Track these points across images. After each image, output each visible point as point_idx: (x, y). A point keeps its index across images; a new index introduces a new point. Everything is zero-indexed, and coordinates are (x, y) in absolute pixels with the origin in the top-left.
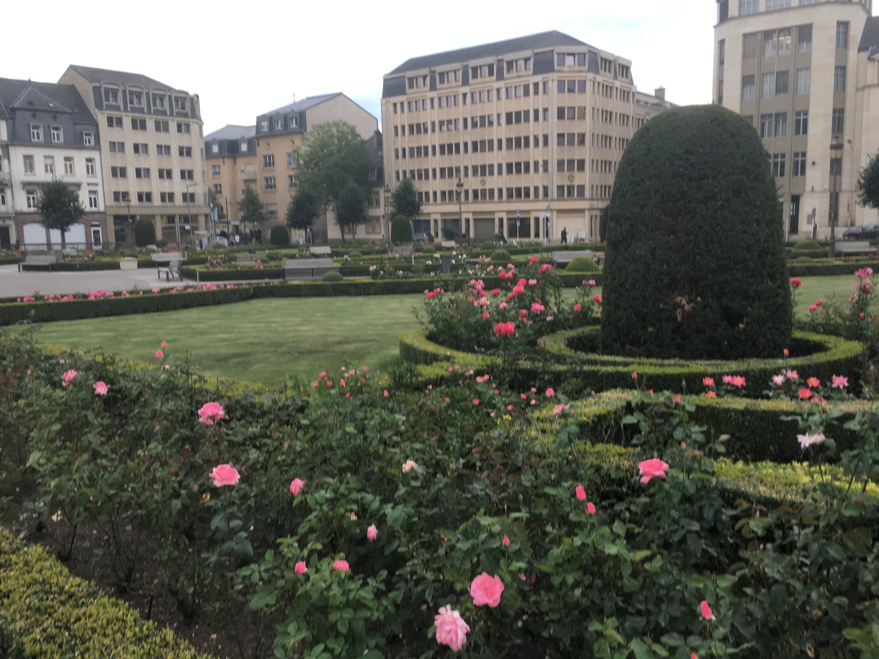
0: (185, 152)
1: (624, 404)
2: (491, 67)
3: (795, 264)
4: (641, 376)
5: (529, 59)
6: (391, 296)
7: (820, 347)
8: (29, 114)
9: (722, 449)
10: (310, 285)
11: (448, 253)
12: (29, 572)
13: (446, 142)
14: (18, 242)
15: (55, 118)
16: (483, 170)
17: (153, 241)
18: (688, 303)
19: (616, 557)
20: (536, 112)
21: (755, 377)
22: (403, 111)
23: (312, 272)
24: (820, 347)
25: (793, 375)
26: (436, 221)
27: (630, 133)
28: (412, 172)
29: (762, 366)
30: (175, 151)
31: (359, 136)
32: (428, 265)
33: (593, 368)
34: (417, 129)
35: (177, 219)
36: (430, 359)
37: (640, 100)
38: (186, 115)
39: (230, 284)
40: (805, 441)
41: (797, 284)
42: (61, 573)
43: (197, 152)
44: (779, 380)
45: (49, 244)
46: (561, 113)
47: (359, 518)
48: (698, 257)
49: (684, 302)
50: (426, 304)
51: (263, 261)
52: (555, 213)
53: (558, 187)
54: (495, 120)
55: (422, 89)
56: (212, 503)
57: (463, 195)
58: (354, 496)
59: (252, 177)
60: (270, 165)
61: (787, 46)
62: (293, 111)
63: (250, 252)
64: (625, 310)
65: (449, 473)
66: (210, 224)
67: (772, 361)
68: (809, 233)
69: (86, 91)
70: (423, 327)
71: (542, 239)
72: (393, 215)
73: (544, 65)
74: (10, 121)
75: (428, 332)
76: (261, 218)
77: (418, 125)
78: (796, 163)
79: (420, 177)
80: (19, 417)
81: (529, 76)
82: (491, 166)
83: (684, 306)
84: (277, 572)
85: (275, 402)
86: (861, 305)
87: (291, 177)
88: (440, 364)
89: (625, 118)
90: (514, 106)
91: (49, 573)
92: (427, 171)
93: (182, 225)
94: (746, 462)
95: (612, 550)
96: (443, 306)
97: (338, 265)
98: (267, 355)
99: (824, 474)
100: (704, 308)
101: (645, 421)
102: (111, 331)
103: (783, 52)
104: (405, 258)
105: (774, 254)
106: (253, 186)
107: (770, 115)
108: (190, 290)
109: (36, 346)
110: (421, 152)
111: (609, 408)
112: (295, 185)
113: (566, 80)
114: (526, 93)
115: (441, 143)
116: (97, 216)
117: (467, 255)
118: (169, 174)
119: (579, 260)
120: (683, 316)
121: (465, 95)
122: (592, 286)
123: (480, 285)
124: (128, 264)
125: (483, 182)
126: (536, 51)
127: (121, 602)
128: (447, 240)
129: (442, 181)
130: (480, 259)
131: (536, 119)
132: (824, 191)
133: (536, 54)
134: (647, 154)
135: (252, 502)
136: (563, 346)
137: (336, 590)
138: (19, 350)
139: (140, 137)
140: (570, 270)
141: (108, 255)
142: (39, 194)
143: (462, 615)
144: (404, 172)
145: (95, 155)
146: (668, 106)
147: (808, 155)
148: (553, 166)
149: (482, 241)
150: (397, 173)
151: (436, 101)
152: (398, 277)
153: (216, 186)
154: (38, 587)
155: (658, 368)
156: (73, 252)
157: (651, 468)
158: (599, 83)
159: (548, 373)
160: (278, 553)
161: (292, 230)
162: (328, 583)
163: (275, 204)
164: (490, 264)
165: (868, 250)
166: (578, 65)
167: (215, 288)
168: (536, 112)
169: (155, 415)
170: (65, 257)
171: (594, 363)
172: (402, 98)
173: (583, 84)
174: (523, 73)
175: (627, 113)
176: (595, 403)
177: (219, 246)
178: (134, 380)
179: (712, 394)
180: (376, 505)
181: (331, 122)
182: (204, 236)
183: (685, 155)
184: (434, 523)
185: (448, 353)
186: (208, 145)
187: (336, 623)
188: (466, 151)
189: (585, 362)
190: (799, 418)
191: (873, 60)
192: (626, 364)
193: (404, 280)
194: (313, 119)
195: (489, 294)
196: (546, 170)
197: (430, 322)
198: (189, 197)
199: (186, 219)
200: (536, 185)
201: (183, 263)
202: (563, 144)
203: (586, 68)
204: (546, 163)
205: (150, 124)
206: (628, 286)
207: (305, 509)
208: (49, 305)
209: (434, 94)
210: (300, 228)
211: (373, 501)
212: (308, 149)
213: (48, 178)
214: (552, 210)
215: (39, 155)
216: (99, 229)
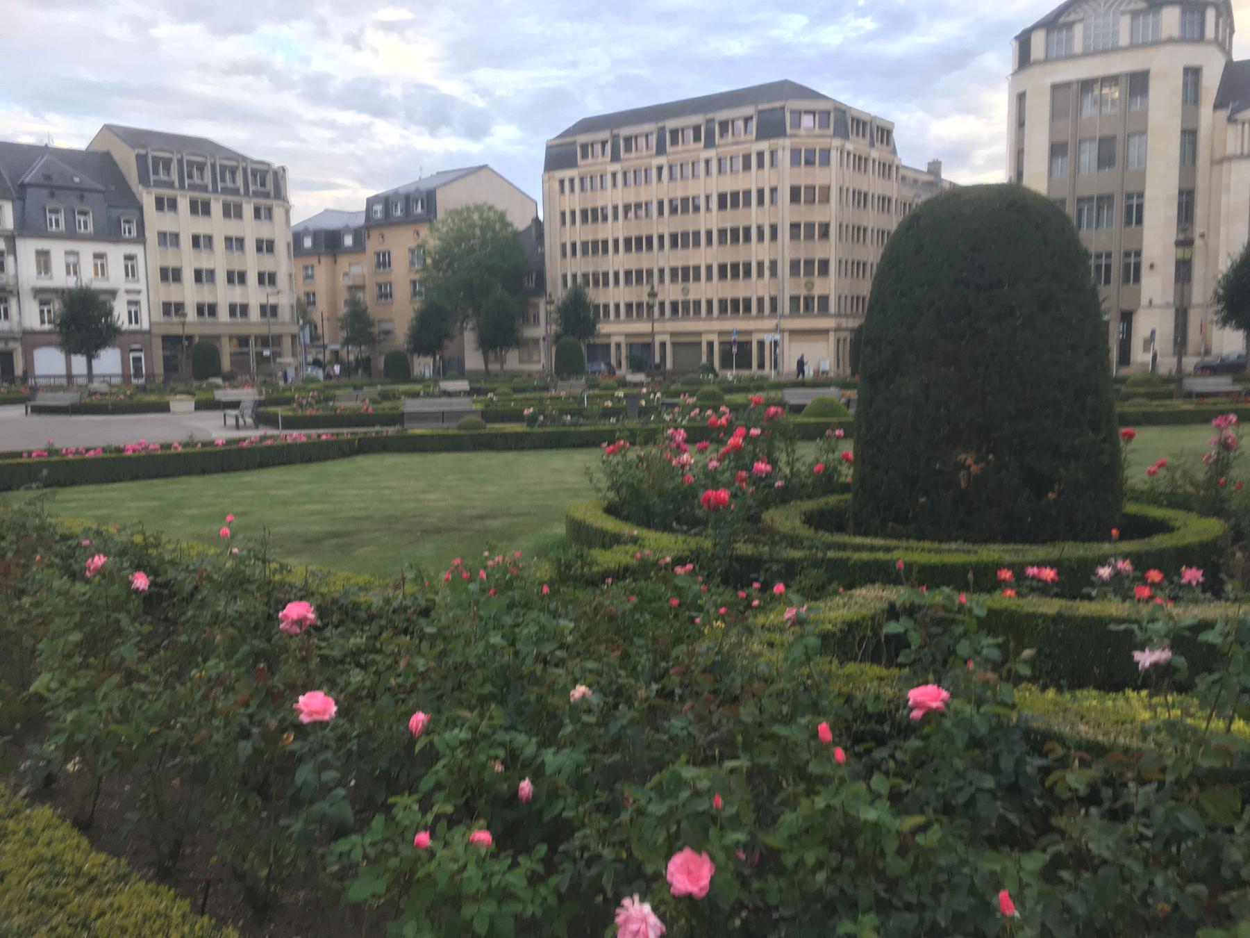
0: (264, 246)
1: (886, 606)
6: (554, 451)
7: (1162, 527)
8: (45, 192)
10: (439, 436)
11: (635, 391)
12: (32, 845)
13: (633, 235)
14: (25, 373)
15: (82, 198)
16: (686, 274)
17: (217, 372)
18: (976, 462)
20: (761, 193)
22: (572, 190)
23: (443, 416)
24: (1162, 527)
25: (1125, 566)
26: (618, 346)
27: (892, 222)
28: (585, 276)
29: (1081, 552)
30: (250, 245)
31: (511, 225)
33: (840, 554)
34: (592, 215)
35: (252, 341)
36: (610, 541)
37: (906, 178)
38: (267, 195)
39: (325, 434)
40: (1145, 659)
41: (1130, 437)
42: (78, 846)
43: (281, 247)
44: (1105, 572)
45: (70, 376)
46: (795, 194)
47: (507, 768)
49: (969, 461)
51: (373, 401)
52: (786, 335)
56: (296, 746)
58: (501, 736)
59: (359, 282)
60: (384, 266)
61: (1113, 101)
62: (417, 190)
63: (355, 387)
65: (636, 704)
66: (299, 349)
68: (1144, 365)
69: (127, 160)
71: (768, 371)
72: (558, 337)
73: (771, 127)
74: (18, 203)
76: (371, 341)
77: (594, 211)
78: (1127, 266)
79: (596, 283)
80: (22, 622)
81: (751, 142)
83: (969, 467)
84: (388, 847)
85: (387, 601)
86: (1220, 466)
87: (414, 283)
88: (622, 547)
89: (885, 201)
90: (729, 184)
91: (62, 846)
92: (606, 275)
93: (259, 349)
94: (1060, 690)
95: (870, 814)
96: (629, 465)
97: (480, 407)
98: (377, 534)
102: (154, 499)
103: (1108, 110)
104: (575, 398)
106: (360, 295)
107: (1090, 199)
108: (269, 442)
109: (49, 520)
110: (597, 248)
111: (864, 612)
112: (420, 293)
114: (747, 166)
115: (626, 234)
116: (139, 337)
117: (663, 394)
118: (242, 278)
120: (969, 481)
121: (660, 169)
122: (839, 438)
124: (182, 405)
125: (685, 291)
127: (163, 889)
128: (633, 372)
129: (627, 289)
131: (761, 202)
132: (1167, 305)
133: (760, 113)
135: (353, 745)
136: (798, 522)
137: (472, 871)
138: (23, 526)
139: (202, 226)
141: (152, 391)
142: (57, 306)
143: (655, 909)
144: (574, 276)
145: (137, 250)
146: (947, 186)
148: (784, 269)
149: (684, 373)
150: (565, 277)
151: (620, 177)
152: (564, 424)
153: (308, 295)
154: (45, 867)
156: (104, 388)
158: (848, 154)
159: (778, 561)
160: (390, 819)
161: (415, 357)
162: (461, 863)
163: (391, 320)
164: (694, 407)
166: (820, 126)
167: (304, 439)
168: (761, 193)
169: (216, 620)
170: (92, 394)
171: (843, 547)
172: (573, 173)
173: (826, 154)
174: (742, 137)
175: (888, 194)
176: (845, 605)
177: (312, 380)
178: (187, 570)
180: (530, 749)
181: (472, 206)
182: (289, 365)
184: (614, 776)
185: (636, 532)
186: (298, 237)
187: (472, 919)
188: (661, 246)
193: (572, 429)
194: (447, 201)
195: (693, 449)
196: (774, 273)
198: (269, 311)
199: (265, 341)
201: (259, 404)
204: (773, 264)
205: (216, 208)
207: (431, 755)
208: (68, 462)
209: (617, 167)
210: (426, 355)
211: (526, 744)
212: (437, 242)
213: (71, 282)
214: (782, 331)
215: (58, 250)
216: (142, 355)
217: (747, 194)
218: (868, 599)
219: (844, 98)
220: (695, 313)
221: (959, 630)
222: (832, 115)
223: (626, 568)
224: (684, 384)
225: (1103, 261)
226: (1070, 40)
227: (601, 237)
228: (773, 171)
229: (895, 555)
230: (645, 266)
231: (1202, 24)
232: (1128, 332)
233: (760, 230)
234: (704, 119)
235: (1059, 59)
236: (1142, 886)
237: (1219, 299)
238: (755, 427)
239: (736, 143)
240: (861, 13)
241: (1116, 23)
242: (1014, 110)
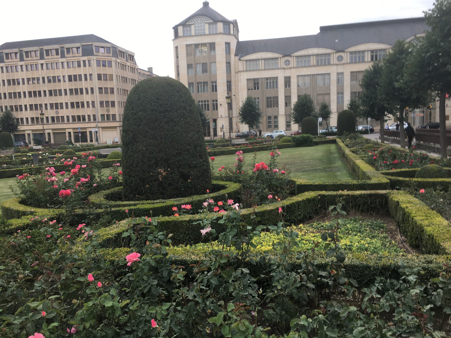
2: (57, 50)
3: (216, 150)
4: (130, 210)
5: (79, 48)
7: (224, 187)
9: (170, 241)
11: (37, 153)
16: (56, 106)
19: (112, 307)
20: (86, 75)
24: (224, 187)
25: (212, 201)
26: (29, 135)
29: (199, 198)
33: (117, 209)
36: (19, 215)
37: (140, 72)
40: (203, 232)
41: (213, 160)
44: (206, 204)
50: (18, 183)
52: (100, 129)
53: (101, 115)
55: (15, 60)
57: (45, 120)
61: (205, 51)
71: (94, 143)
73: (88, 51)
77: (14, 80)
78: (214, 104)
79: (17, 110)
86: (239, 167)
90: (72, 72)
95: (109, 304)
96: (29, 182)
99: (216, 246)
100: (172, 173)
101: (134, 233)
103: (204, 54)
104: (8, 157)
105: (201, 146)
110: (17, 95)
114: (79, 66)
120: (162, 178)
122: (118, 166)
123: (52, 170)
125: (57, 113)
126: (83, 44)
130: (56, 155)
131: (86, 79)
133: (83, 45)
134: (139, 100)
136: (102, 199)
140: (109, 159)
144: (6, 107)
146: (155, 76)
148: (97, 104)
155: (151, 205)
157: (132, 257)
158: (119, 63)
159: (92, 214)
171: (119, 206)
174: (76, 55)
179: (177, 215)
183: (157, 101)
189: (114, 206)
191: (241, 60)
192: (135, 205)
195: (58, 174)
196: (94, 106)
202: (102, 93)
203: (111, 55)
204: (93, 102)
206: (135, 165)
209: (22, 63)
220: (62, 122)
221: (149, 231)
222: (111, 48)
223: (28, 225)
224: (59, 149)
226: (190, 30)
228: (90, 68)
229: (138, 207)
230: (38, 103)
232: (216, 126)
233: (87, 89)
235: (187, 36)
237: (240, 115)
239: (74, 57)
241: (204, 26)
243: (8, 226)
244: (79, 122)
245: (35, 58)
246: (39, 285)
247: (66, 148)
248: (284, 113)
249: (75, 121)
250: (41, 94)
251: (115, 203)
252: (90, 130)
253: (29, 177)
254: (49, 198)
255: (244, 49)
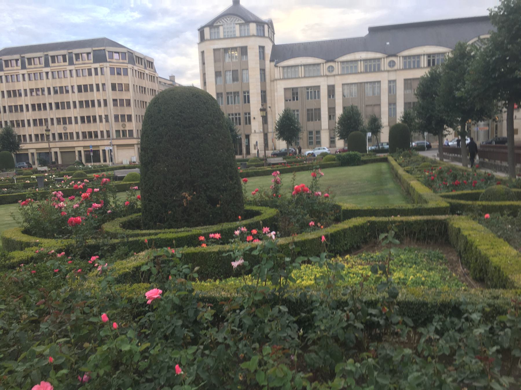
2: (64, 56)
3: (248, 171)
5: (90, 53)
7: (258, 213)
9: (196, 275)
11: (42, 175)
16: (65, 121)
19: (130, 351)
20: (98, 85)
21: (226, 233)
24: (258, 213)
25: (244, 229)
26: (33, 154)
29: (230, 226)
32: (28, 183)
33: (135, 239)
36: (22, 246)
40: (235, 264)
41: (246, 181)
44: (237, 232)
48: (192, 170)
49: (187, 195)
50: (20, 210)
52: (115, 147)
53: (116, 131)
54: (70, 89)
55: (15, 68)
57: (51, 137)
61: (236, 57)
64: (155, 202)
65: (22, 321)
67: (234, 223)
68: (255, 154)
70: (20, 225)
71: (108, 163)
73: (99, 57)
75: (23, 228)
77: (14, 91)
78: (246, 118)
79: (18, 125)
82: (70, 118)
86: (276, 190)
94: (221, 280)
95: (126, 348)
96: (33, 209)
99: (249, 281)
101: (154, 267)
103: (234, 60)
104: (9, 180)
107: (231, 93)
110: (18, 109)
113: (115, 67)
114: (90, 74)
117: (56, 175)
119: (130, 175)
122: (136, 190)
125: (65, 129)
126: (94, 49)
128: (41, 166)
129: (35, 128)
130: (64, 178)
132: (261, 132)
133: (94, 51)
136: (118, 227)
140: (125, 181)
144: (6, 122)
146: (177, 85)
147: (251, 114)
148: (112, 119)
149: (67, 165)
155: (174, 234)
157: (153, 293)
158: (136, 71)
159: (106, 245)
165: (282, 162)
171: (137, 235)
173: (126, 71)
174: (87, 61)
179: (204, 245)
183: (180, 114)
185: (38, 241)
190: (232, 253)
192: (156, 234)
195: (67, 200)
196: (107, 121)
197: (25, 221)
200: (102, 130)
203: (127, 61)
206: (155, 189)
209: (24, 71)
214: (113, 145)
217: (91, 86)
218: (141, 259)
219: (130, 46)
220: (71, 138)
221: (171, 264)
223: (32, 258)
224: (67, 170)
225: (238, 116)
226: (218, 33)
227: (19, 103)
228: (102, 76)
231: (264, 31)
234: (68, 52)
235: (215, 39)
236: (234, 349)
238: (97, 188)
239: (84, 64)
240: (133, 10)
241: (234, 27)
242: (201, 58)
243: (9, 259)
244: (91, 139)
245: (39, 66)
246: (46, 327)
247: (75, 169)
248: (327, 127)
249: (86, 137)
250: (46, 107)
251: (132, 233)
252: (103, 148)
253: (33, 202)
254: (58, 227)
255: (281, 53)
